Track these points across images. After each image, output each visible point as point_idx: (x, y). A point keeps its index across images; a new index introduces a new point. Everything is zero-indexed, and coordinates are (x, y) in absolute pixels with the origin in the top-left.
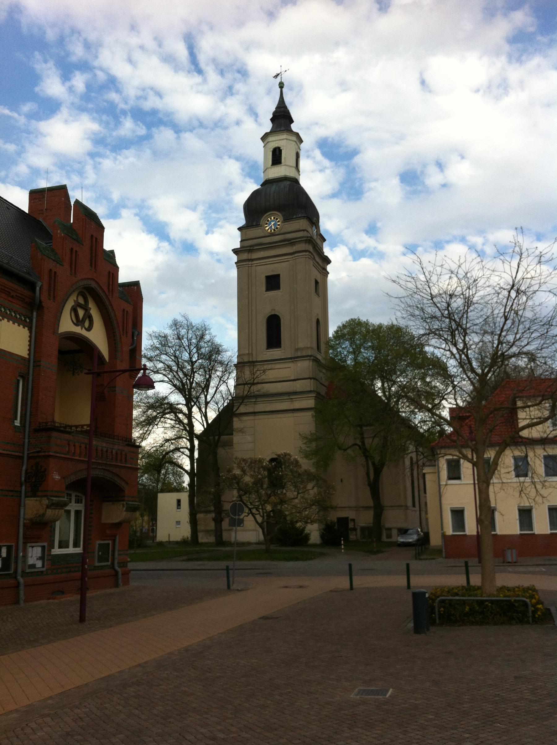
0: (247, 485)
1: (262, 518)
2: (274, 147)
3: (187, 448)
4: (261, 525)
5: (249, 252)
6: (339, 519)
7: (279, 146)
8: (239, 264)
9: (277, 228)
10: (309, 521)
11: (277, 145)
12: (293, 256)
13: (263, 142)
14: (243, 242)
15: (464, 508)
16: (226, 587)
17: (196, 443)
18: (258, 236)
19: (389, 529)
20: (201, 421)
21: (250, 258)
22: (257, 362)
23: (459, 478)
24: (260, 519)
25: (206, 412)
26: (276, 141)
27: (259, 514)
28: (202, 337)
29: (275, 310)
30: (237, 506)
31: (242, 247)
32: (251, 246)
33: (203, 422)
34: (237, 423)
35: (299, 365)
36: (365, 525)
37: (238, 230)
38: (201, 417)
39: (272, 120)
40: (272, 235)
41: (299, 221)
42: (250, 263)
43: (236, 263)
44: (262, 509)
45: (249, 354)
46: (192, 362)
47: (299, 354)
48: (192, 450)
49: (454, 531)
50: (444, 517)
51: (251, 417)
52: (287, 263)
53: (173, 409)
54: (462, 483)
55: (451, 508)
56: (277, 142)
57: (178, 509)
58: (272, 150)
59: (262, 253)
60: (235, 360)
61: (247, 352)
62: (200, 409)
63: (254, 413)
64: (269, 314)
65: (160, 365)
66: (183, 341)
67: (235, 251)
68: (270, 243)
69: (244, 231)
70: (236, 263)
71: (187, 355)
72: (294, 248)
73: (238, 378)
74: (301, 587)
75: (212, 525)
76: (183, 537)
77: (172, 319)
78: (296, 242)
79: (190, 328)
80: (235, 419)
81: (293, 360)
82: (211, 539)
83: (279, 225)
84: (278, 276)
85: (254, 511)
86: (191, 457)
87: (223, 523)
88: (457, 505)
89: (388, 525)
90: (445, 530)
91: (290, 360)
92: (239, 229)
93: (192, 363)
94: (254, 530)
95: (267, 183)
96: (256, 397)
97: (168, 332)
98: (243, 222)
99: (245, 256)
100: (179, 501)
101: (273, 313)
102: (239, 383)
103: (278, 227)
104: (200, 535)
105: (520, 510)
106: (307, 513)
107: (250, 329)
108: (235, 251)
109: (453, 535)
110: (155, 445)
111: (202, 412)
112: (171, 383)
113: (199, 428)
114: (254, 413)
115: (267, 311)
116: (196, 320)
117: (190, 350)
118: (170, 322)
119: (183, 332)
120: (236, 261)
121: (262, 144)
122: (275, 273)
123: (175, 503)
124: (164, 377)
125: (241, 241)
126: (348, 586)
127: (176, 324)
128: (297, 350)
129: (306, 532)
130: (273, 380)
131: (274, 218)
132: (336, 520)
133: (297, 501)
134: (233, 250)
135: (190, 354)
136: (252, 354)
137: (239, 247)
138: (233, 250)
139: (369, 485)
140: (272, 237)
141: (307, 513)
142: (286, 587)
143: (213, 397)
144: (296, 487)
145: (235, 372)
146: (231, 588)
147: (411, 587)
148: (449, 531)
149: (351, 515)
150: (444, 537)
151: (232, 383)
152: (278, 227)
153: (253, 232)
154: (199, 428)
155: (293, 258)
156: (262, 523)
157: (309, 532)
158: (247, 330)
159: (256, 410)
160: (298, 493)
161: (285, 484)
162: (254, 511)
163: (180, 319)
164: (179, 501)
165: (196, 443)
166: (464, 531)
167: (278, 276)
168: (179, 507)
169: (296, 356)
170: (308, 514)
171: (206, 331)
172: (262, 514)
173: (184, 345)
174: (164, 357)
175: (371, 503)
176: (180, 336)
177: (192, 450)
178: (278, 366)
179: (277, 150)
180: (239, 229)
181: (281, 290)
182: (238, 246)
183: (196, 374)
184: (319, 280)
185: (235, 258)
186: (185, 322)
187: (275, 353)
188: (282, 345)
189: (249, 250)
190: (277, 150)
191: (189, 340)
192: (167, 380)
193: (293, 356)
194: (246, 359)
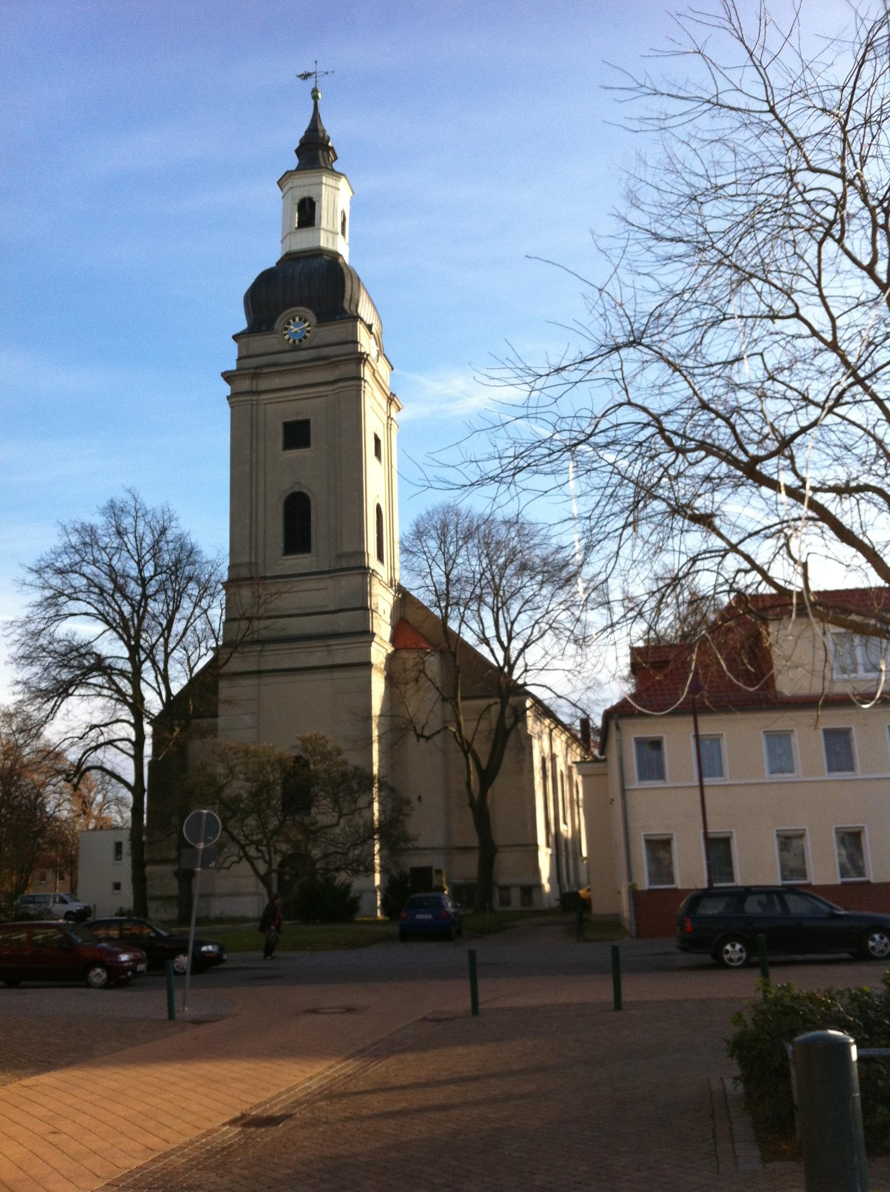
0: (238, 799)
1: (266, 865)
2: (301, 197)
3: (129, 740)
4: (265, 879)
5: (253, 378)
6: (413, 870)
7: (311, 195)
8: (234, 400)
9: (305, 337)
10: (362, 868)
11: (306, 194)
12: (335, 386)
13: (282, 189)
14: (242, 361)
15: (672, 834)
16: (165, 1015)
17: (148, 729)
18: (269, 350)
19: (506, 888)
20: (155, 685)
21: (254, 389)
22: (265, 578)
23: (661, 776)
24: (262, 868)
25: (166, 669)
26: (304, 186)
27: (263, 857)
28: (163, 531)
29: (299, 484)
30: (204, 819)
31: (238, 369)
32: (256, 368)
33: (159, 687)
34: (225, 690)
35: (343, 584)
36: (461, 881)
37: (233, 341)
38: (156, 677)
39: (298, 152)
40: (295, 348)
41: (322, 584)
42: (255, 398)
43: (228, 398)
44: (268, 846)
45: (250, 563)
46: (143, 579)
47: (344, 564)
48: (138, 744)
49: (650, 884)
50: (633, 851)
51: (251, 681)
52: (323, 399)
53: (101, 666)
54: (667, 785)
55: (646, 835)
56: (306, 188)
57: (117, 859)
58: (297, 201)
59: (277, 380)
60: (223, 573)
61: (247, 560)
62: (154, 663)
63: (259, 673)
64: (289, 493)
65: (79, 582)
66: (126, 539)
67: (228, 377)
68: (294, 363)
69: (243, 340)
70: (228, 398)
71: (135, 565)
72: (337, 372)
73: (229, 607)
74: (350, 1010)
75: (173, 887)
76: (122, 908)
77: (108, 498)
78: (339, 361)
79: (139, 514)
80: (222, 684)
81: (333, 575)
82: (172, 913)
83: (309, 332)
84: (307, 423)
85: (252, 851)
86: (138, 757)
87: (193, 880)
88: (658, 830)
89: (502, 880)
90: (635, 880)
91: (327, 576)
92: (236, 337)
93: (143, 582)
94: (253, 894)
95: (289, 258)
96: (263, 642)
97: (99, 521)
98: (241, 323)
99: (245, 385)
100: (119, 846)
101: (297, 490)
102: (233, 617)
103: (307, 334)
104: (152, 906)
105: (778, 836)
106: (357, 852)
107: (254, 517)
108: (228, 377)
109: (650, 891)
110: (69, 735)
111: (158, 667)
112: (100, 617)
113: (154, 703)
114: (259, 673)
115: (285, 485)
116: (152, 501)
117: (139, 556)
118: (103, 503)
119: (127, 522)
120: (229, 394)
121: (279, 193)
122: (301, 418)
123: (112, 849)
124: (89, 606)
125: (239, 359)
126: (468, 1004)
127: (114, 510)
128: (339, 557)
129: (352, 895)
130: (296, 612)
131: (300, 319)
132: (408, 871)
133: (337, 830)
134: (223, 374)
135: (138, 563)
136: (256, 564)
137: (235, 368)
138: (223, 374)
139: (472, 805)
140: (297, 353)
141: (357, 852)
142: (314, 1011)
143: (181, 640)
144: (336, 801)
145: (224, 592)
146: (177, 1015)
147: (624, 1006)
148: (644, 884)
149: (435, 861)
150: (635, 895)
151: (217, 614)
152: (307, 334)
153: (261, 343)
154: (154, 703)
155: (333, 390)
156: (268, 873)
157: (358, 895)
158: (247, 521)
159: (264, 667)
160: (341, 816)
161: (316, 795)
162: (252, 851)
163: (121, 496)
164: (119, 846)
165: (148, 729)
166: (672, 881)
167: (307, 423)
168: (118, 857)
169: (338, 567)
170: (359, 855)
171: (170, 521)
172: (267, 857)
173: (130, 546)
174: (88, 569)
175: (473, 840)
176: (121, 530)
177: (138, 744)
178: (304, 586)
179: (307, 203)
180: (236, 337)
181: (312, 448)
182: (232, 366)
183: (150, 601)
184: (380, 437)
185: (226, 389)
186: (132, 503)
187: (300, 562)
188: (313, 548)
189: (254, 374)
190: (307, 203)
191: (139, 540)
192: (95, 612)
193: (332, 568)
194: (245, 572)
